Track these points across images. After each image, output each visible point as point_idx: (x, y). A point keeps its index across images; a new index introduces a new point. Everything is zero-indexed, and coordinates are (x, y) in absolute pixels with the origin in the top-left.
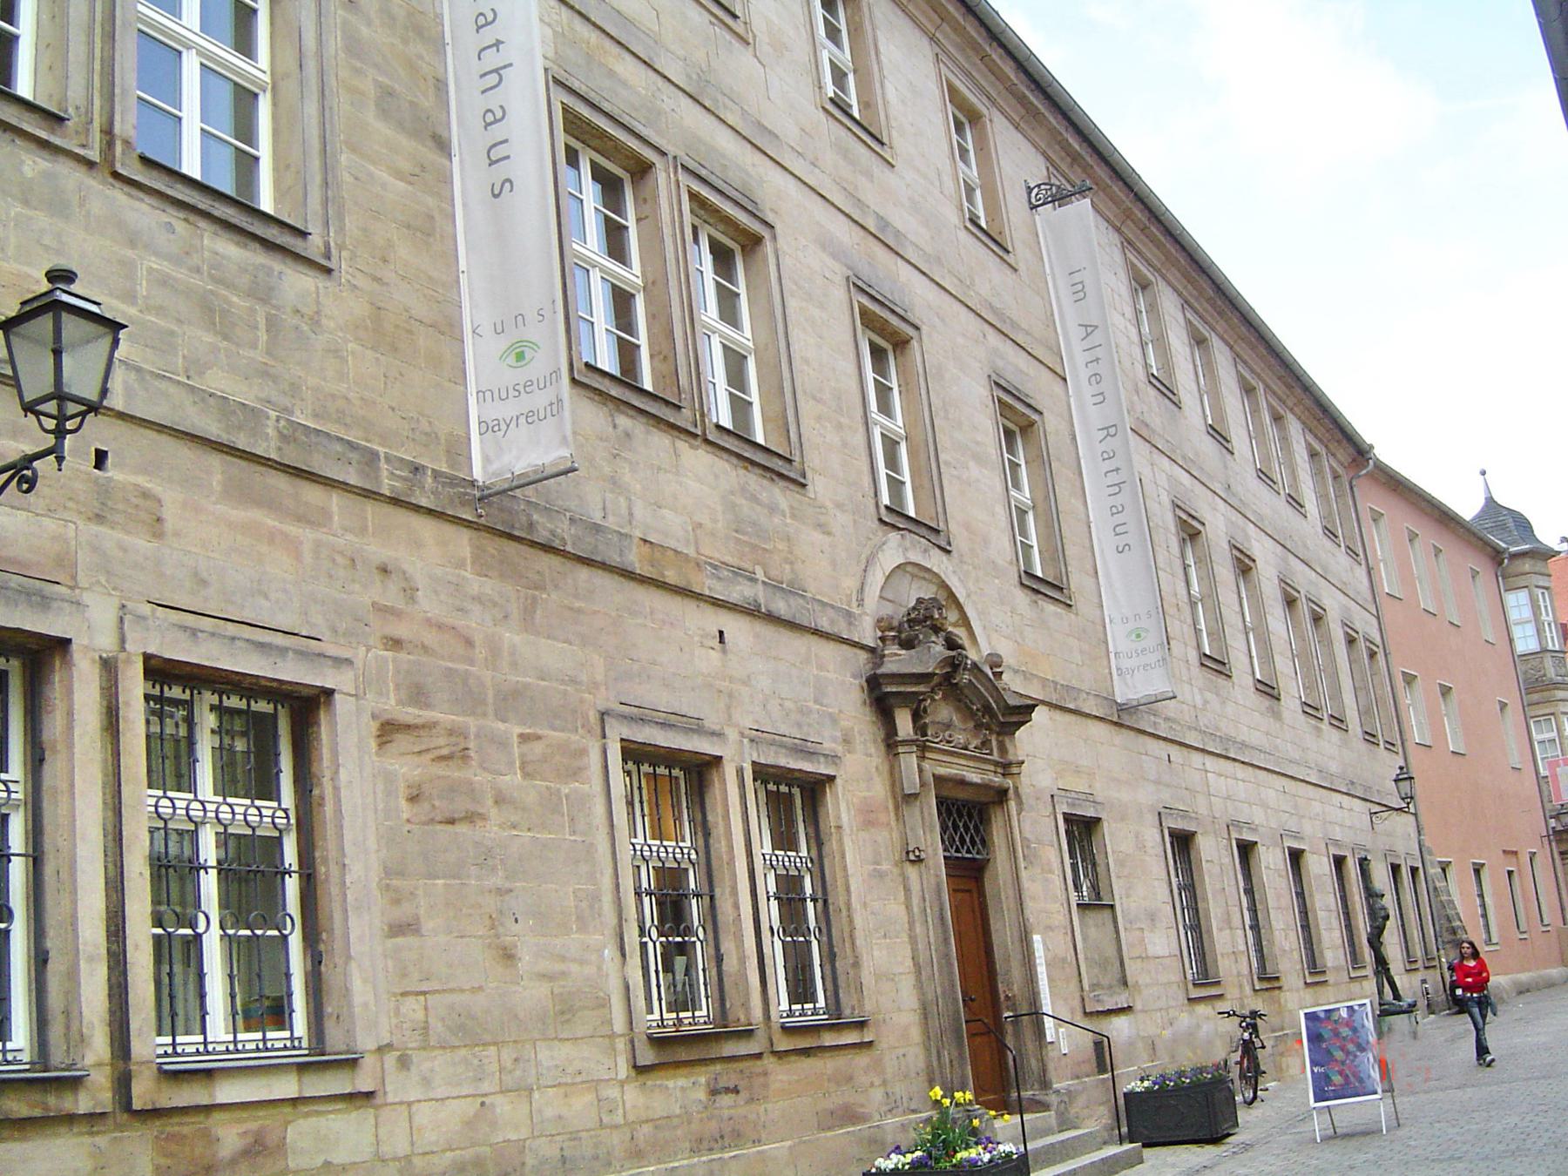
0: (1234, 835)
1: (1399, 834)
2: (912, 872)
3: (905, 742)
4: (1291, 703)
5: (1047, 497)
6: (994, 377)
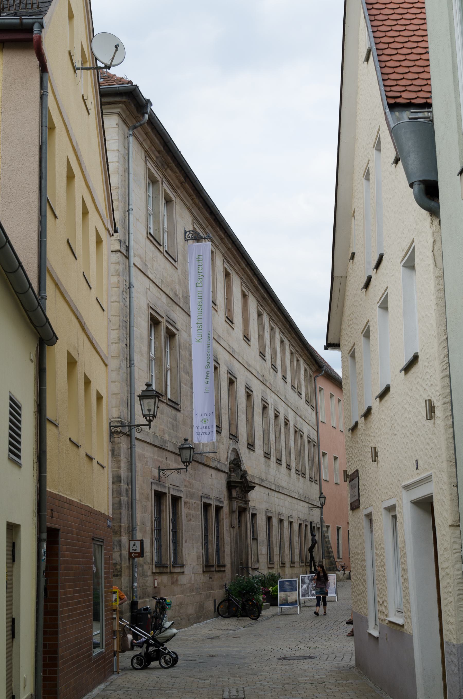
0: (279, 517)
1: (315, 516)
2: (232, 530)
3: (234, 498)
4: (293, 470)
5: (252, 418)
6: (247, 386)
